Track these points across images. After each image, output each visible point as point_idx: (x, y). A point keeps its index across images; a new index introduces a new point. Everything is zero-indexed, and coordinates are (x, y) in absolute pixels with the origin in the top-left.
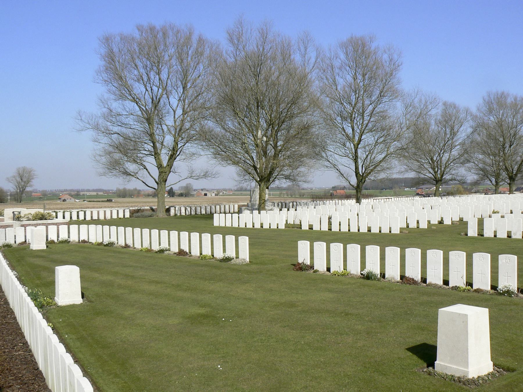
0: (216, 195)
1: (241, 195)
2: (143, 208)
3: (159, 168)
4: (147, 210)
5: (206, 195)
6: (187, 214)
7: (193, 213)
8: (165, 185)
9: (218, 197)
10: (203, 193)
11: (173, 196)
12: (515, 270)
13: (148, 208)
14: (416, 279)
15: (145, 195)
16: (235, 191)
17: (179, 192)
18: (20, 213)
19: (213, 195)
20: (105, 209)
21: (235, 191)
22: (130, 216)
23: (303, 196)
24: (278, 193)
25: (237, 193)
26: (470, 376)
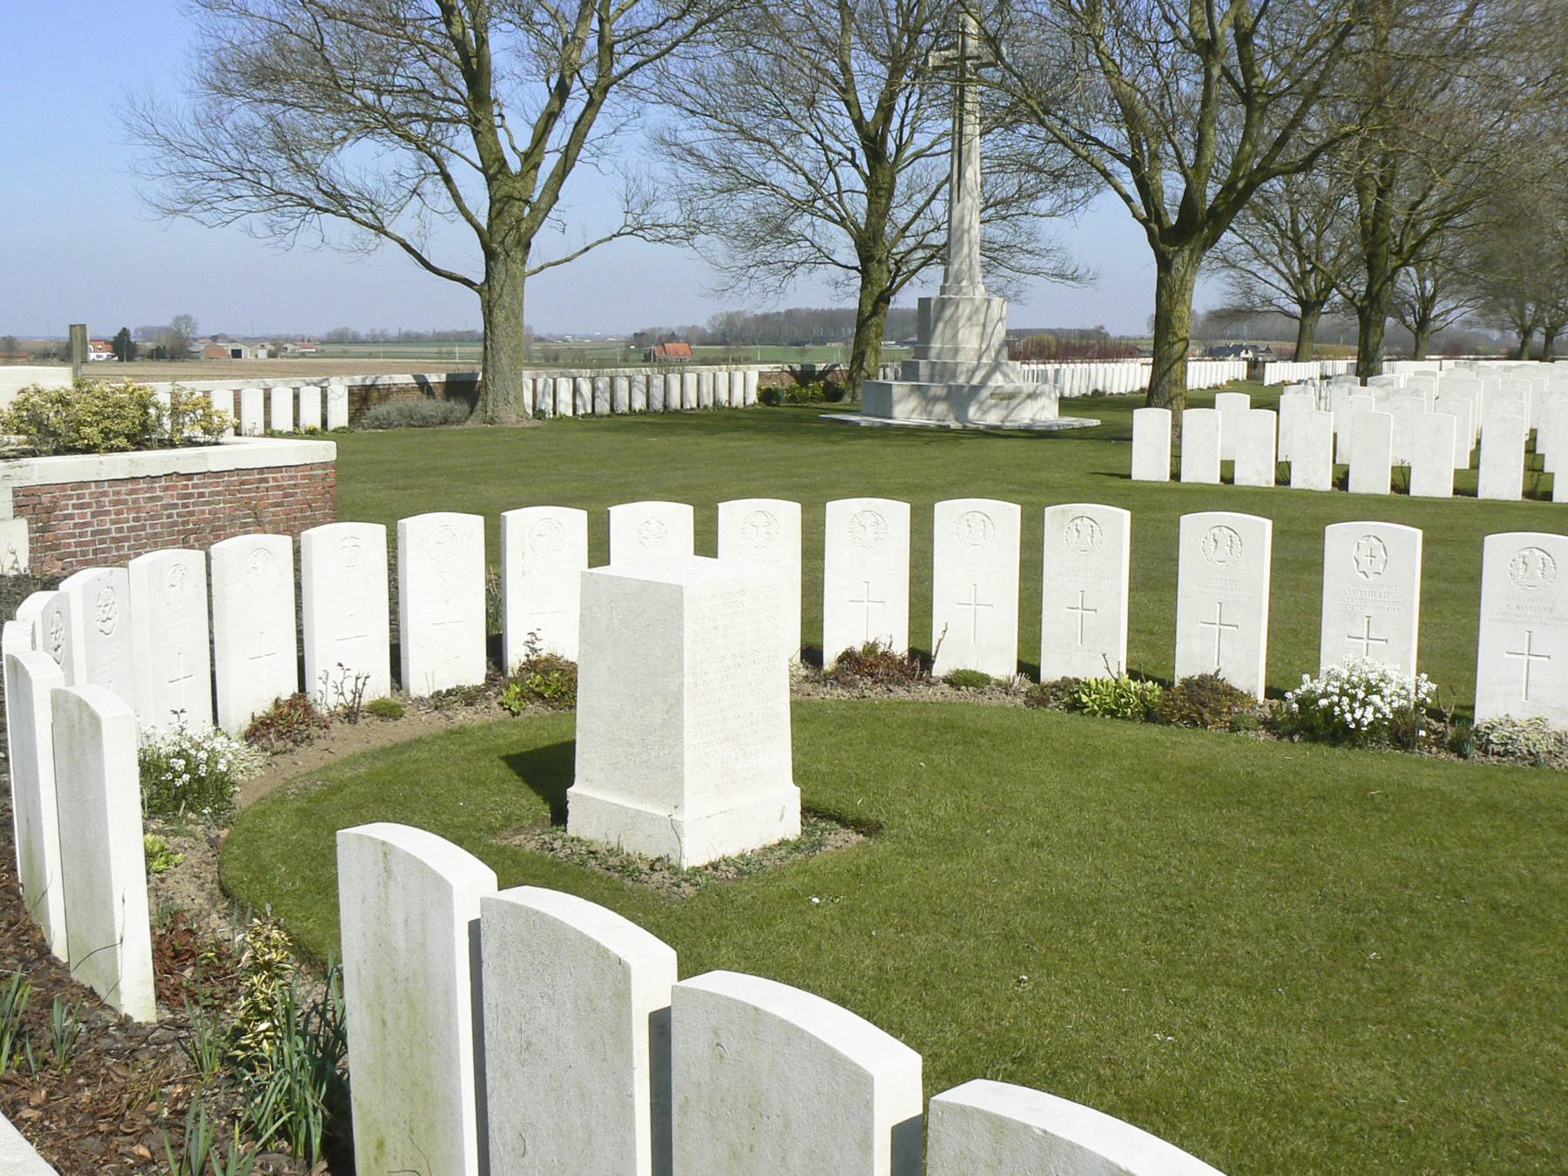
0: (272, 355)
1: (345, 355)
2: (385, 380)
3: (490, 180)
4: (403, 390)
5: (237, 354)
6: (581, 412)
7: (603, 407)
8: (524, 262)
9: (278, 360)
10: (230, 348)
11: (130, 359)
12: (1261, 608)
13: (406, 379)
14: (1239, 682)
15: (30, 353)
16: (323, 343)
17: (150, 345)
18: (207, 394)
19: (263, 354)
20: (297, 382)
21: (323, 343)
22: (352, 419)
23: (556, 359)
24: (435, 350)
25: (329, 348)
26: (694, 856)
